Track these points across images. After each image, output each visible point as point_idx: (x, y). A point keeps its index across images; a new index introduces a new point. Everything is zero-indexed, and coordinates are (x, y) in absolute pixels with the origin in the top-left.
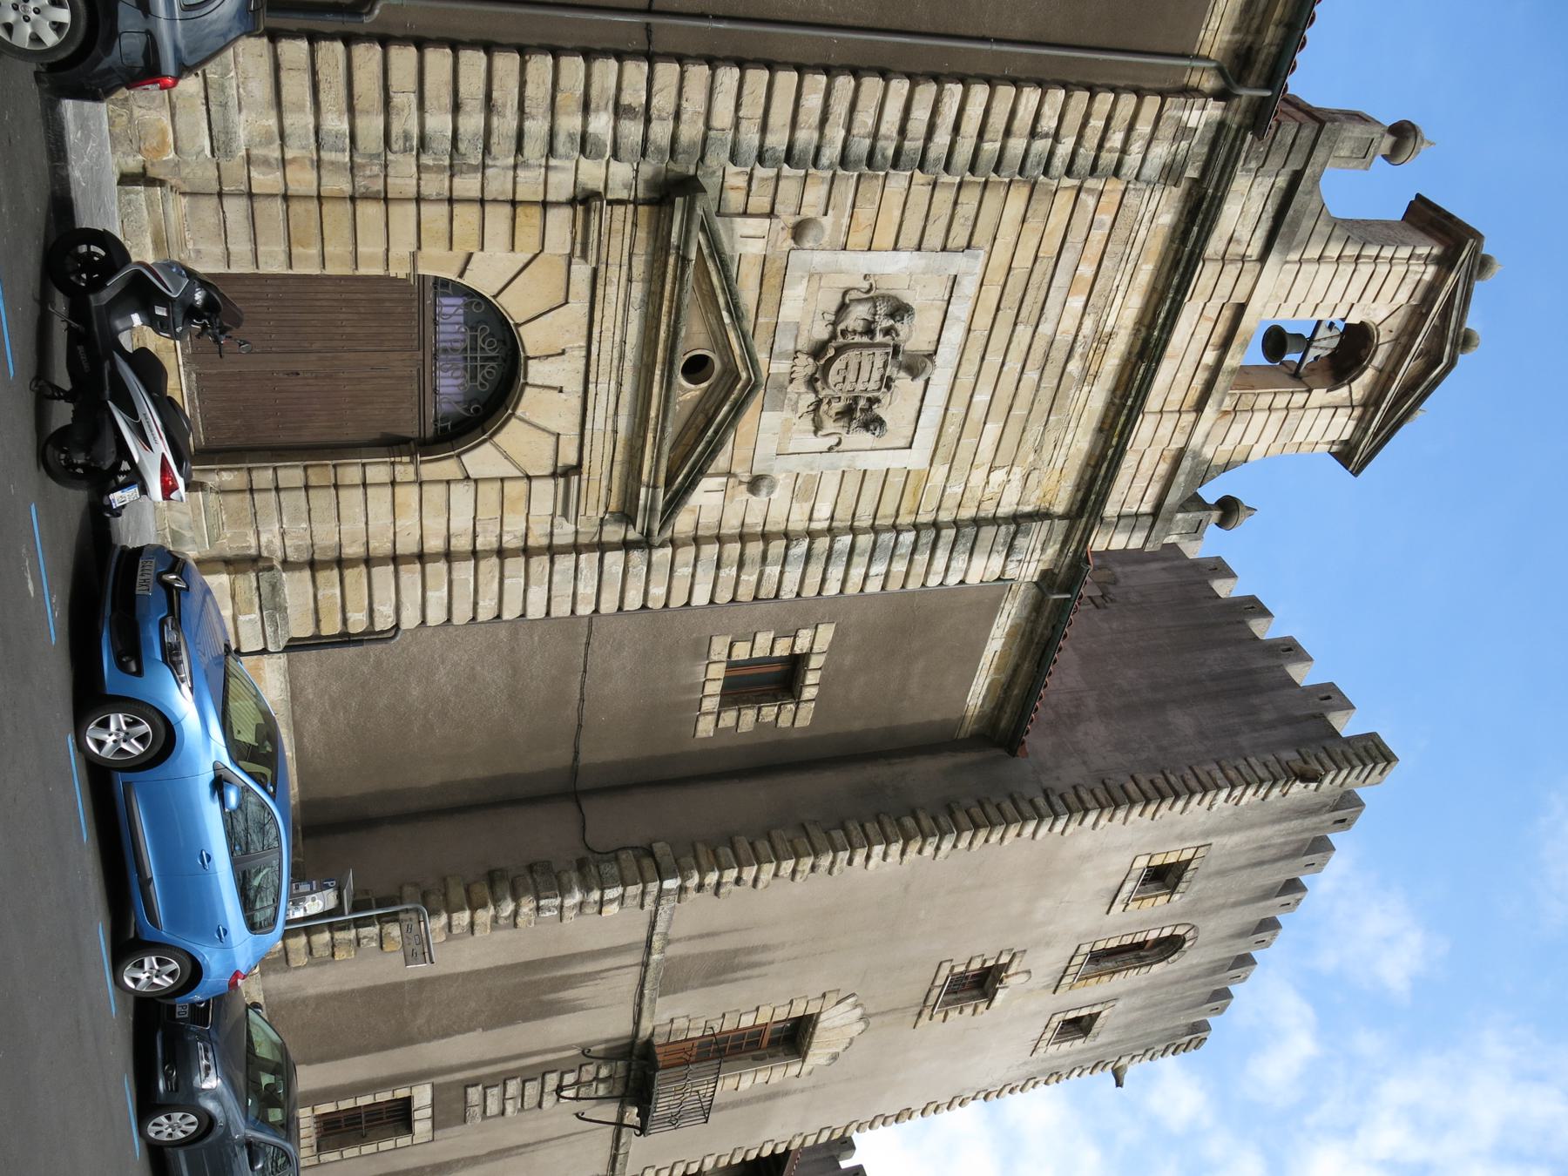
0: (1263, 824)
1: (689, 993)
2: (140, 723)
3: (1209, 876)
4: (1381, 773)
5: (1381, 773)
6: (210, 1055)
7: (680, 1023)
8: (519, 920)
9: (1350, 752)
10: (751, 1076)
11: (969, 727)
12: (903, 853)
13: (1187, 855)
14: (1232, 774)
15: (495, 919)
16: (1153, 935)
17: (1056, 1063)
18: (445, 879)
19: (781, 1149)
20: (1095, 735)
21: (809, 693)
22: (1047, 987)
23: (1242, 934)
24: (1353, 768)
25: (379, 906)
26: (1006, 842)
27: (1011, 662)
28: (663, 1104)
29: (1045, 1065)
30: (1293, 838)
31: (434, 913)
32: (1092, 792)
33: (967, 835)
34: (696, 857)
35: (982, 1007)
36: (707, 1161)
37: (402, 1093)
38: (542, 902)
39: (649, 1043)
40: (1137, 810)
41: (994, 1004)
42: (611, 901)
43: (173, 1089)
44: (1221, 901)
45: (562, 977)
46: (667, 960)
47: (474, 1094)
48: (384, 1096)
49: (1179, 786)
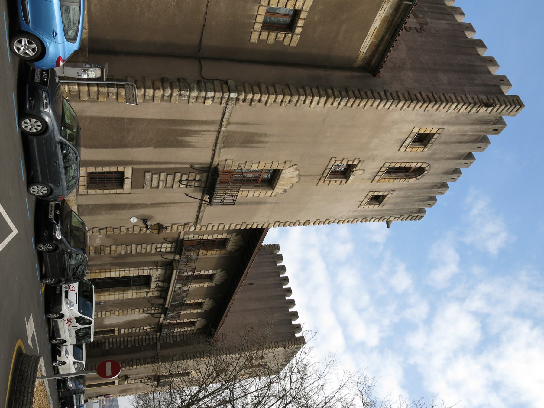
0: (466, 124)
1: (234, 149)
2: (33, 44)
3: (440, 143)
4: (516, 111)
5: (516, 111)
6: (48, 99)
7: (229, 162)
8: (172, 98)
9: (507, 100)
10: (253, 192)
11: (359, 62)
12: (325, 103)
13: (434, 131)
14: (459, 99)
15: (163, 96)
16: (414, 165)
17: (366, 213)
18: (144, 78)
19: (259, 227)
20: (408, 76)
21: (298, 30)
22: (369, 179)
23: (447, 173)
24: (506, 106)
25: (117, 81)
26: (366, 108)
27: (381, 34)
28: (219, 194)
29: (362, 214)
30: (476, 133)
31: (139, 88)
32: (403, 95)
33: (352, 100)
34: (244, 88)
35: (344, 182)
36: (232, 225)
37: (120, 169)
38: (182, 92)
39: (216, 168)
40: (419, 105)
41: (349, 181)
42: (209, 98)
43: (33, 107)
44: (442, 156)
45: (186, 130)
46: (228, 132)
47: (148, 175)
48: (114, 169)
49: (438, 99)
